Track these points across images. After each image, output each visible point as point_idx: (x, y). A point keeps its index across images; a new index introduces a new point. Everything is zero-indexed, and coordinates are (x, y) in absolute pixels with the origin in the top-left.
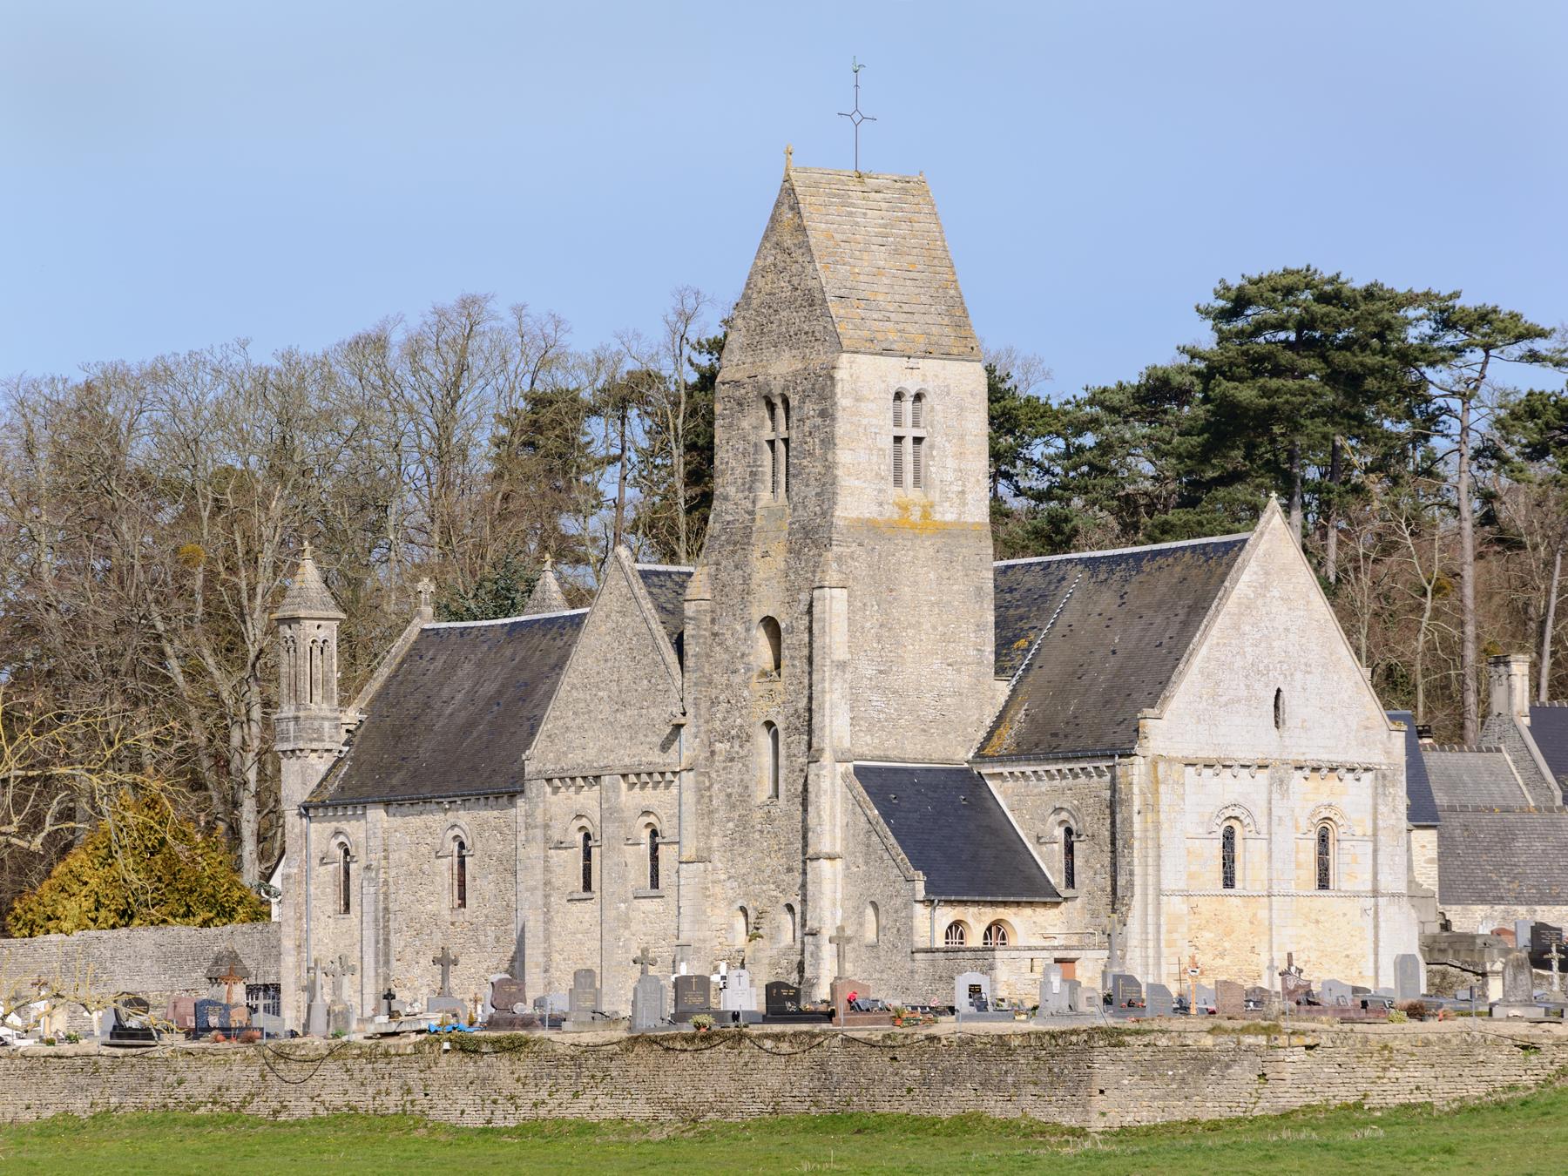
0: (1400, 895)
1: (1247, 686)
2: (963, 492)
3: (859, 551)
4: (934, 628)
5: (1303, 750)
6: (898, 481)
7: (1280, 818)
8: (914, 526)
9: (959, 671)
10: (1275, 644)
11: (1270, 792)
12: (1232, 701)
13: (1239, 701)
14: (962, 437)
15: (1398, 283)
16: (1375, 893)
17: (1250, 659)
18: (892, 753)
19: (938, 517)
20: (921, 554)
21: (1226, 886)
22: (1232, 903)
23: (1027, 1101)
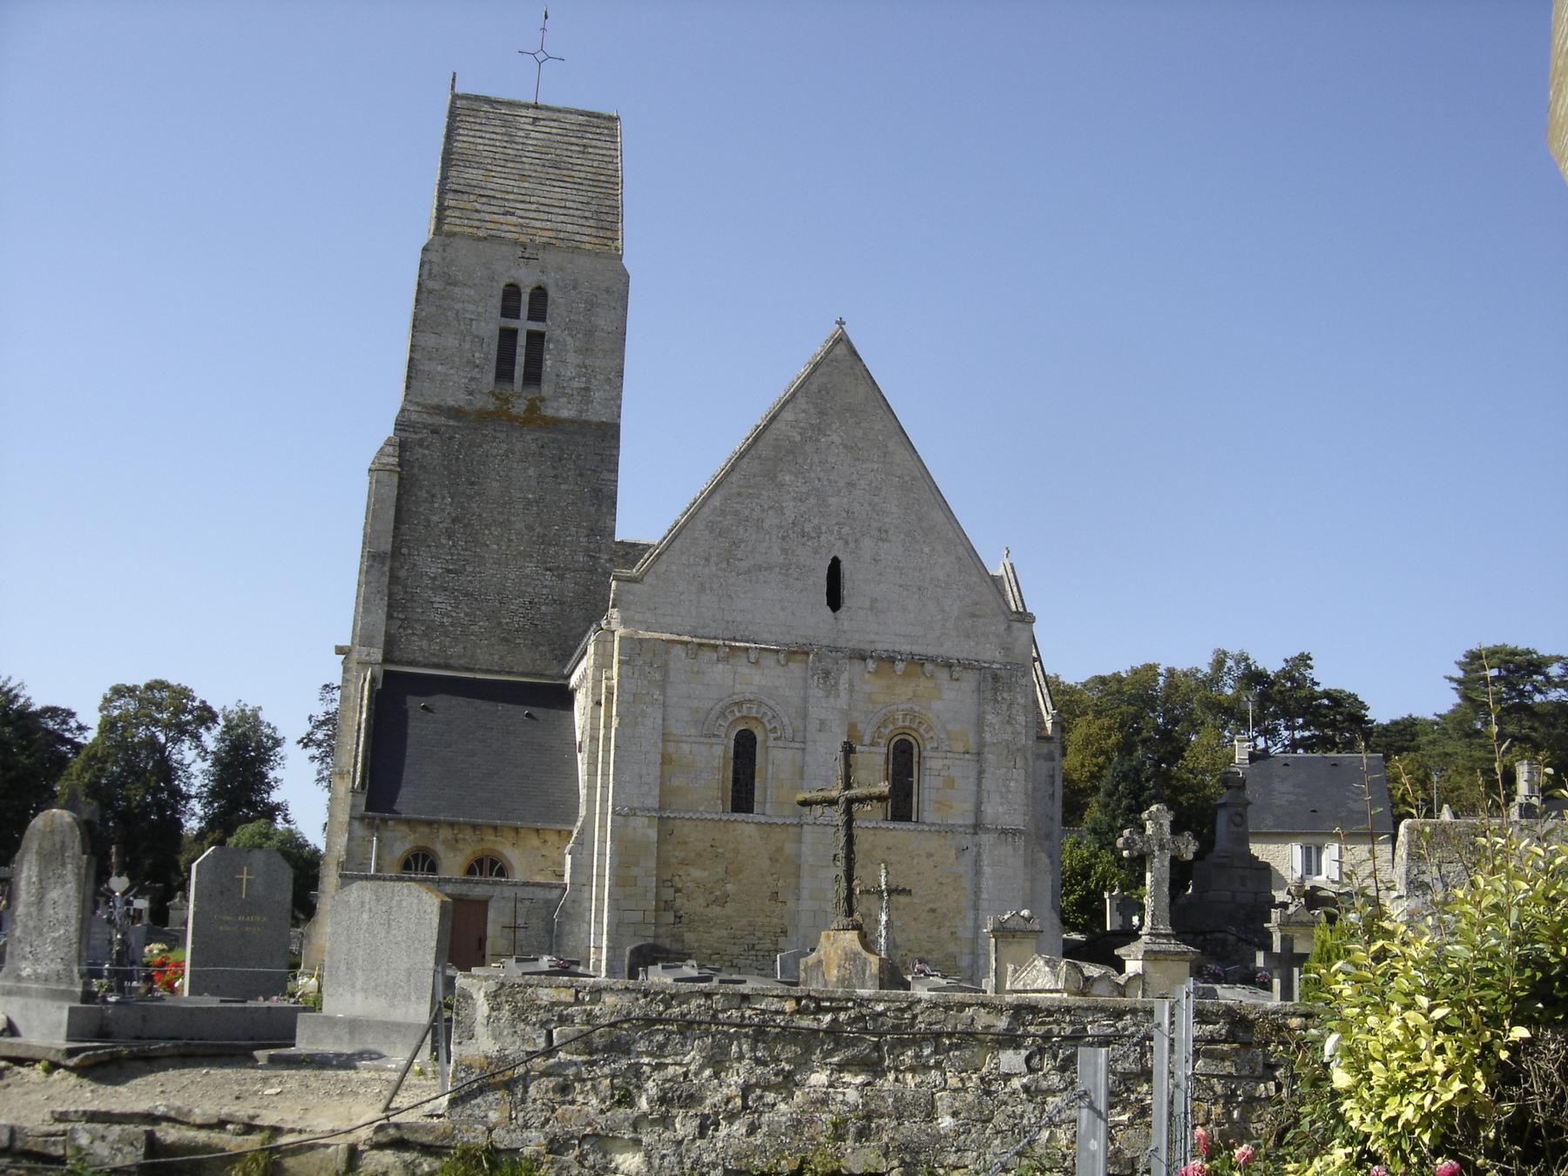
0: (1015, 832)
1: (784, 551)
2: (587, 389)
4: (530, 528)
5: (873, 637)
7: (822, 722)
8: (512, 419)
9: (561, 577)
10: (832, 500)
11: (806, 687)
13: (770, 568)
14: (590, 333)
15: (1544, 650)
16: (977, 827)
17: (790, 515)
19: (549, 412)
21: (736, 808)
22: (745, 828)
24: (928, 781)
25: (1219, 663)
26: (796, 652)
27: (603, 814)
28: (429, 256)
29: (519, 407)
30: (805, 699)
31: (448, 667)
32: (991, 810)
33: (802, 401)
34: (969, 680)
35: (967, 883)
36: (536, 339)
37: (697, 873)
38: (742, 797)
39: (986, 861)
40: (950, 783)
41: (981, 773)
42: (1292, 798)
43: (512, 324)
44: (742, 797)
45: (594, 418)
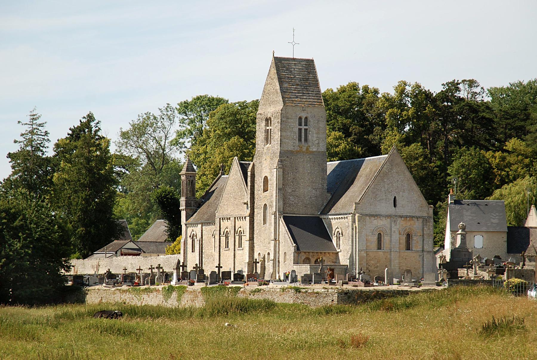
3: (287, 159)
4: (309, 179)
6: (300, 140)
8: (303, 152)
9: (316, 191)
12: (381, 200)
14: (318, 129)
16: (423, 251)
18: (296, 213)
19: (311, 150)
20: (305, 159)
22: (380, 253)
23: (74, 312)
24: (414, 242)
25: (402, 92)
26: (389, 216)
27: (356, 251)
28: (283, 112)
29: (304, 149)
30: (391, 226)
31: (294, 214)
32: (426, 247)
33: (388, 163)
34: (421, 220)
35: (421, 263)
36: (300, 124)
37: (372, 262)
38: (379, 248)
39: (425, 258)
40: (417, 242)
41: (423, 240)
42: (471, 218)
43: (301, 127)
44: (379, 248)
45: (321, 150)
